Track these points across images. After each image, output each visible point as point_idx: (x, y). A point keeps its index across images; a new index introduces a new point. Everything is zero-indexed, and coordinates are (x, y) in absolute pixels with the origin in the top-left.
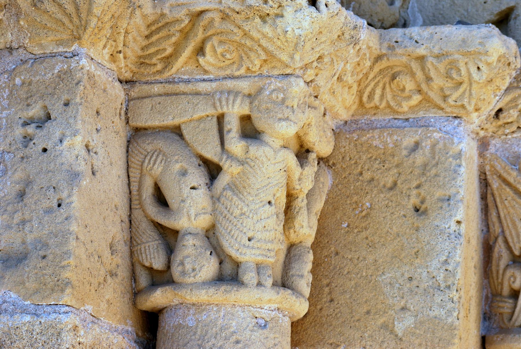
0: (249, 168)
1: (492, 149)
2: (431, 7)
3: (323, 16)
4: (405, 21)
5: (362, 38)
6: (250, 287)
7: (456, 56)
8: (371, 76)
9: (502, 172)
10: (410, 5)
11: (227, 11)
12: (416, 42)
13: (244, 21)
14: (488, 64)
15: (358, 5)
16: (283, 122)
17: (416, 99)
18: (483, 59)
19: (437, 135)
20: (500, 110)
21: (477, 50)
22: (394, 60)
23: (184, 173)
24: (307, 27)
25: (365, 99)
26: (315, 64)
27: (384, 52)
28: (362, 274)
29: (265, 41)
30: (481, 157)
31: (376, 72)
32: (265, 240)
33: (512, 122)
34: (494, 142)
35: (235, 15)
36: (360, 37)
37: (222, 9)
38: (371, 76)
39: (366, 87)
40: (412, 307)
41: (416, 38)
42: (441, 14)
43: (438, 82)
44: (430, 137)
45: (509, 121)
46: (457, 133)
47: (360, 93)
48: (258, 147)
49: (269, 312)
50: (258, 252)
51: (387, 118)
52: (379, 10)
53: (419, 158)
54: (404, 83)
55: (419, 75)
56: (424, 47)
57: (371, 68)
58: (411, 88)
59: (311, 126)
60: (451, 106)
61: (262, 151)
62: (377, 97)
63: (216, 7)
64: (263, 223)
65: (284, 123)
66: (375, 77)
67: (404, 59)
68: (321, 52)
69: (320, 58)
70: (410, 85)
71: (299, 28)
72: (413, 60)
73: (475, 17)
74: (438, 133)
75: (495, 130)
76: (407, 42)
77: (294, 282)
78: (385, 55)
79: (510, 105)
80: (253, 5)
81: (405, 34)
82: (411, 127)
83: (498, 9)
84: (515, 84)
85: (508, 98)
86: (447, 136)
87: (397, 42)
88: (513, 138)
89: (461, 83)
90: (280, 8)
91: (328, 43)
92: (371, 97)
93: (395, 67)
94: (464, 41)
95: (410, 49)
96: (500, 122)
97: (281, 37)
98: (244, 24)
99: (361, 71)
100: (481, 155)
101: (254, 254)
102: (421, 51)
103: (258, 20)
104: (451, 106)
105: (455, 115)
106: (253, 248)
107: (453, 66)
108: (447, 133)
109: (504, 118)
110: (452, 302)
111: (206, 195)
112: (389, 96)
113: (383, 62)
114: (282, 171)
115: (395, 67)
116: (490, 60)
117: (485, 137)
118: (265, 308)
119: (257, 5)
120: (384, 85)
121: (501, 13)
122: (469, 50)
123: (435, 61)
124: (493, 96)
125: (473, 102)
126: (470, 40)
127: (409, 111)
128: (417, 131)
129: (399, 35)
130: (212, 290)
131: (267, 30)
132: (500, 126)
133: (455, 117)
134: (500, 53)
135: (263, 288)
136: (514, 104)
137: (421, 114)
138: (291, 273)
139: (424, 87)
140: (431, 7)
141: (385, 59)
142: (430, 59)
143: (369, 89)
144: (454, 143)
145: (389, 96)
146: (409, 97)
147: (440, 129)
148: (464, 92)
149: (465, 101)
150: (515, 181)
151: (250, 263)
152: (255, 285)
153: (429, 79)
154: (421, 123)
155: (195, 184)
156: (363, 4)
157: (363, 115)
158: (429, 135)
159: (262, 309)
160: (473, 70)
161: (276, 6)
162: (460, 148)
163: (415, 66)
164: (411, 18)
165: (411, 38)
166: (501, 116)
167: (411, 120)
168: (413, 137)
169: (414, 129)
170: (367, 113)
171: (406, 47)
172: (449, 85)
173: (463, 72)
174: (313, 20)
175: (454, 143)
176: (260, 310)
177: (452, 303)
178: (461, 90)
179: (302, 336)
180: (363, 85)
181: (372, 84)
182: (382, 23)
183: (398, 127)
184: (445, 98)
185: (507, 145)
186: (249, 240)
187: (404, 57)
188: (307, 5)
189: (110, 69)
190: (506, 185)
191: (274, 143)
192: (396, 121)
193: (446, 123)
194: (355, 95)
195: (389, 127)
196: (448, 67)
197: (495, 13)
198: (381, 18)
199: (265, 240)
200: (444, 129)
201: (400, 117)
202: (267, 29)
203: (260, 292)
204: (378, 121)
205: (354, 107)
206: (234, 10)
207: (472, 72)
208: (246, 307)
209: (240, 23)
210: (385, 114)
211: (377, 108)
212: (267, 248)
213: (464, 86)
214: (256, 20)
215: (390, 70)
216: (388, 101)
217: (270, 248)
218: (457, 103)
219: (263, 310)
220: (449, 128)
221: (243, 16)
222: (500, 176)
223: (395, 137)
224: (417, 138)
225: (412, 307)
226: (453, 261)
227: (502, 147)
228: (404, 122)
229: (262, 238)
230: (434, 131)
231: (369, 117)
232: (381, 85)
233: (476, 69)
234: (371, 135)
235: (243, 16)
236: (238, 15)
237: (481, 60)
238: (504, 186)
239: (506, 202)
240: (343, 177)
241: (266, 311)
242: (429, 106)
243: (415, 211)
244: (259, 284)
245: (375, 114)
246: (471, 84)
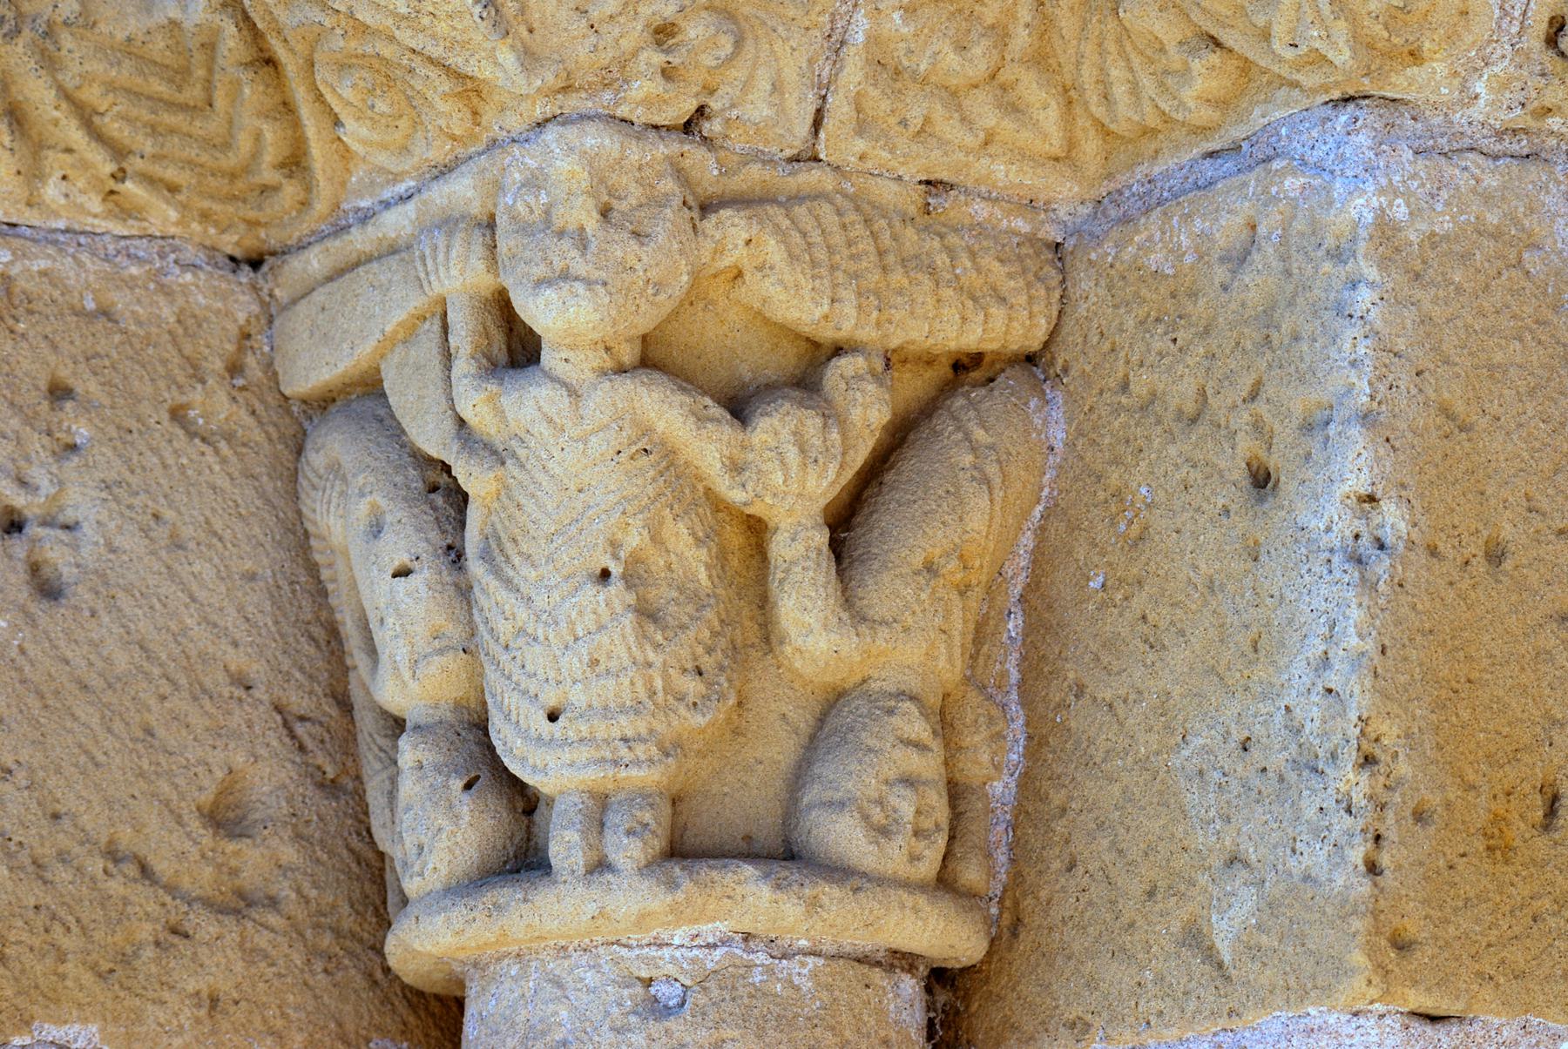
0: (516, 472)
6: (565, 882)
16: (548, 292)
19: (1292, 184)
23: (376, 529)
28: (1137, 752)
29: (409, 32)
32: (606, 708)
40: (1251, 850)
44: (1275, 199)
46: (1342, 158)
48: (522, 392)
49: (695, 952)
50: (584, 753)
51: (1186, 157)
53: (1256, 283)
59: (771, 268)
61: (532, 403)
62: (1120, 91)
64: (584, 651)
65: (550, 294)
74: (1295, 175)
77: (814, 832)
101: (571, 765)
105: (1336, 94)
106: (565, 742)
110: (1349, 811)
111: (439, 587)
112: (1148, 85)
114: (623, 457)
118: (677, 941)
127: (183, 216)
128: (1245, 184)
130: (459, 913)
135: (609, 877)
137: (1257, 120)
138: (805, 800)
143: (1088, 75)
145: (1148, 85)
151: (569, 794)
152: (582, 871)
155: (402, 558)
158: (1274, 190)
159: (660, 946)
176: (652, 952)
177: (1346, 816)
179: (1011, 1009)
186: (553, 717)
189: (141, 237)
191: (568, 367)
199: (606, 708)
203: (596, 892)
204: (1167, 175)
208: (601, 950)
212: (618, 734)
217: (630, 733)
219: (666, 952)
223: (1198, 225)
224: (1246, 208)
225: (1251, 850)
226: (1341, 652)
229: (595, 704)
230: (1282, 173)
234: (1144, 236)
239: (550, 465)
240: (1086, 409)
241: (678, 954)
243: (1255, 487)
244: (600, 866)
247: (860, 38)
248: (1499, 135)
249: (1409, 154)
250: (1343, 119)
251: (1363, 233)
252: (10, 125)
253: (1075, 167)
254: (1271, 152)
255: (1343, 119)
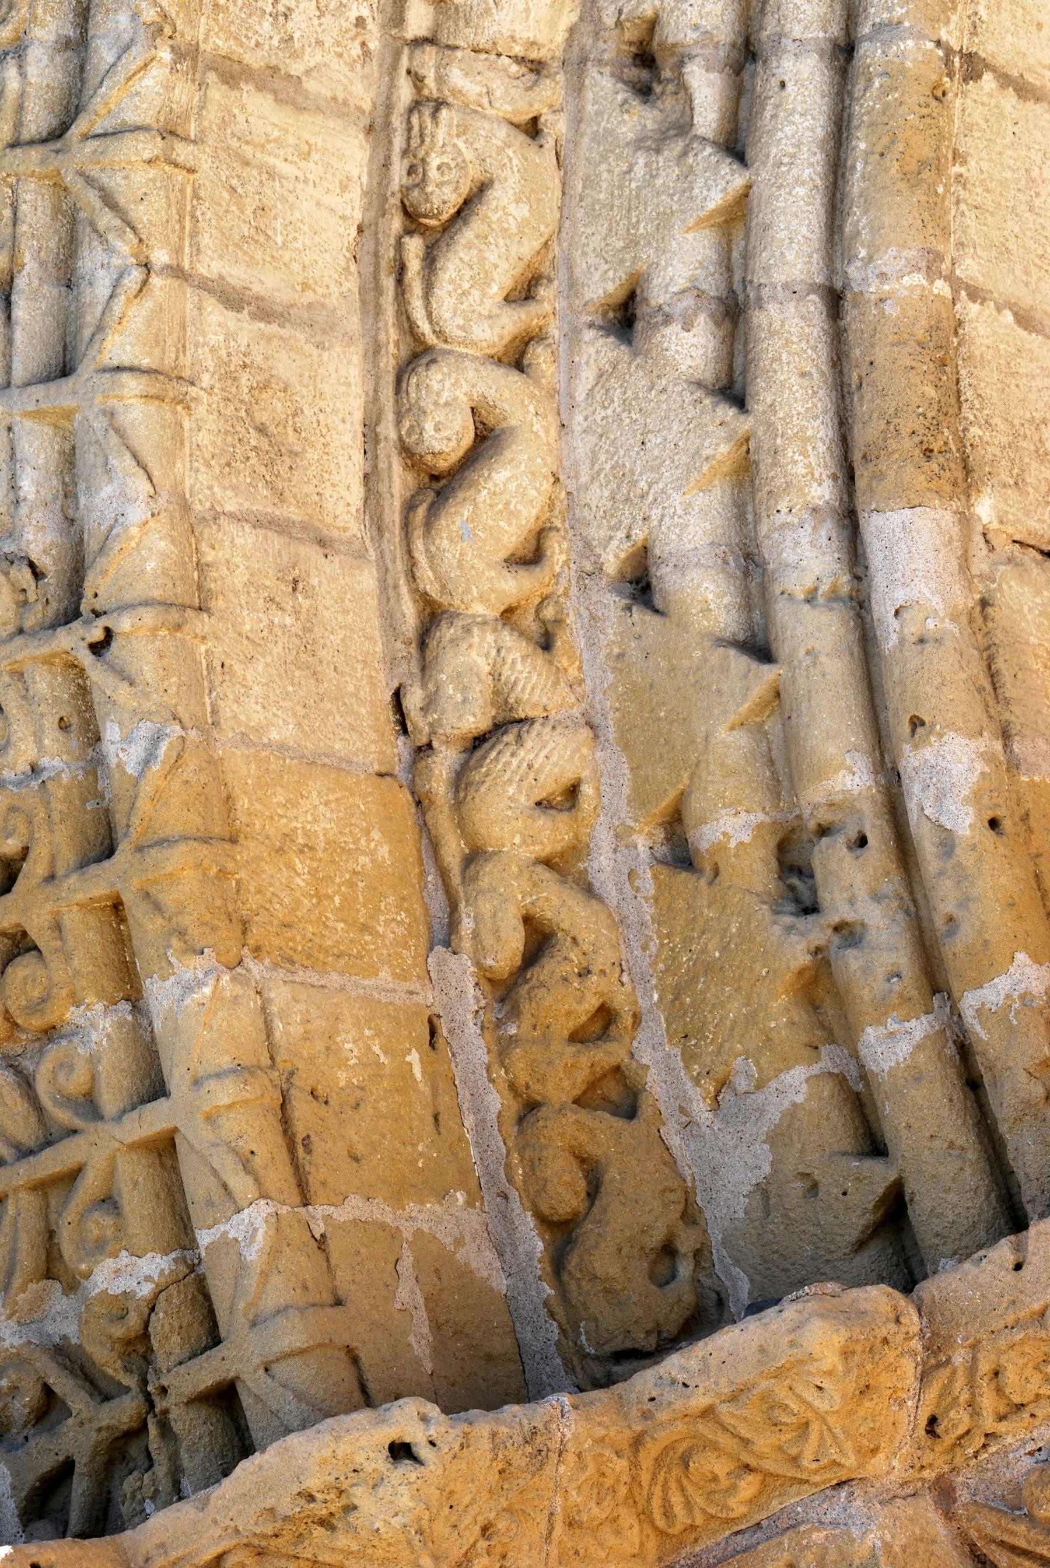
1: (963, 1496)
2: (753, 1244)
3: (433, 1468)
4: (718, 1294)
5: (569, 1435)
7: (764, 1384)
8: (645, 1478)
9: (998, 1534)
10: (715, 1256)
11: (256, 1542)
12: (685, 1385)
13: (296, 1545)
14: (829, 1373)
15: (593, 1325)
17: (748, 1486)
18: (813, 1370)
19: (817, 1537)
20: (933, 1421)
21: (792, 1359)
22: (664, 1436)
24: (411, 1504)
25: (661, 1523)
26: (483, 1544)
27: (639, 1428)
30: (950, 1519)
31: (651, 1468)
33: (968, 1432)
34: (960, 1479)
35: (273, 1542)
36: (564, 1435)
37: (245, 1541)
38: (645, 1478)
39: (649, 1500)
41: (681, 1377)
42: (776, 1252)
43: (764, 1442)
44: (808, 1547)
45: (961, 1431)
46: (850, 1516)
47: (645, 1516)
51: (720, 1538)
52: (639, 1312)
54: (708, 1467)
55: (725, 1441)
56: (701, 1389)
57: (635, 1465)
58: (727, 1470)
60: (815, 1472)
62: (679, 1509)
63: (234, 1542)
66: (654, 1477)
67: (681, 1427)
68: (480, 1519)
69: (485, 1529)
70: (721, 1468)
71: (396, 1514)
72: (699, 1420)
73: (837, 1230)
74: (819, 1530)
75: (948, 1457)
76: (669, 1395)
78: (643, 1433)
79: (943, 1404)
80: (290, 1514)
81: (661, 1378)
82: (768, 1538)
83: (871, 1198)
84: (933, 1361)
85: (932, 1394)
86: (838, 1531)
87: (652, 1399)
88: (993, 1454)
89: (807, 1424)
90: (344, 1495)
91: (485, 1495)
92: (668, 1513)
93: (677, 1445)
94: (762, 1350)
95: (679, 1405)
96: (948, 1440)
97: (376, 1543)
98: (299, 1549)
99: (618, 1480)
100: (949, 1516)
102: (699, 1401)
103: (319, 1532)
104: (815, 1472)
105: (834, 1482)
107: (770, 1405)
108: (835, 1524)
109: (946, 1431)
112: (699, 1501)
113: (648, 1446)
115: (677, 1445)
116: (826, 1365)
117: (940, 1478)
119: (298, 1510)
120: (679, 1481)
121: (882, 1200)
122: (779, 1365)
123: (731, 1408)
124: (896, 1408)
125: (848, 1446)
126: (771, 1343)
128: (781, 1543)
129: (650, 1385)
131: (344, 1541)
132: (953, 1446)
133: (838, 1484)
134: (837, 1345)
136: (949, 1400)
137: (775, 1506)
139: (746, 1458)
140: (753, 1244)
141: (648, 1439)
142: (723, 1409)
143: (656, 1503)
144: (854, 1540)
145: (699, 1501)
146: (733, 1489)
147: (820, 1522)
148: (821, 1437)
149: (833, 1453)
150: (1029, 1542)
153: (746, 1442)
154: (783, 1524)
156: (600, 1318)
157: (677, 1550)
158: (804, 1542)
160: (811, 1395)
161: (332, 1496)
162: (870, 1543)
163: (705, 1429)
164: (728, 1283)
165: (673, 1382)
166: (939, 1430)
167: (764, 1524)
168: (778, 1559)
169: (775, 1541)
170: (681, 1545)
171: (670, 1403)
172: (788, 1436)
173: (794, 1407)
174: (415, 1486)
175: (854, 1540)
178: (814, 1436)
180: (642, 1502)
181: (658, 1490)
182: (659, 1333)
183: (745, 1550)
184: (795, 1460)
185: (990, 1474)
187: (679, 1423)
188: (390, 1466)
190: (1019, 1555)
192: (739, 1537)
193: (825, 1506)
194: (636, 1525)
195: (732, 1556)
196: (764, 1407)
197: (870, 1206)
198: (650, 1326)
200: (827, 1519)
201: (743, 1527)
202: (343, 1541)
204: (708, 1550)
205: (652, 1544)
206: (264, 1536)
207: (810, 1399)
209: (291, 1550)
210: (714, 1533)
211: (693, 1527)
213: (815, 1427)
214: (315, 1533)
215: (671, 1453)
216: (703, 1511)
218: (821, 1463)
220: (832, 1515)
221: (287, 1536)
222: (1002, 1544)
227: (982, 1480)
228: (755, 1532)
230: (809, 1532)
231: (688, 1549)
232: (673, 1485)
233: (814, 1390)
235: (287, 1536)
236: (279, 1540)
237: (810, 1373)
238: (1017, 1560)
242: (781, 1485)
245: (696, 1540)
246: (824, 1421)
247: (559, 1509)
248: (902, 1485)
249: (878, 1506)
250: (843, 1494)
251: (879, 1552)
252: (725, 336)
253: (644, 1559)
254: (793, 1522)
255: (843, 1494)
